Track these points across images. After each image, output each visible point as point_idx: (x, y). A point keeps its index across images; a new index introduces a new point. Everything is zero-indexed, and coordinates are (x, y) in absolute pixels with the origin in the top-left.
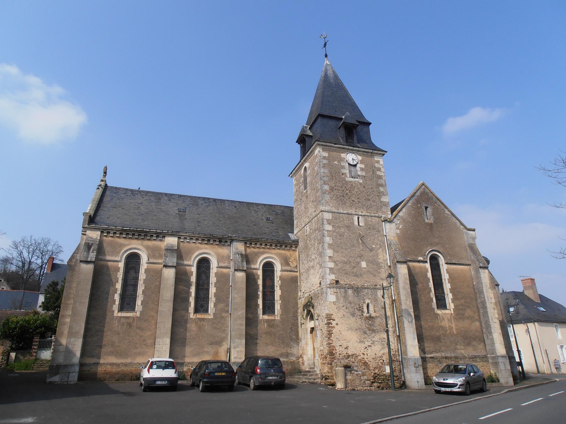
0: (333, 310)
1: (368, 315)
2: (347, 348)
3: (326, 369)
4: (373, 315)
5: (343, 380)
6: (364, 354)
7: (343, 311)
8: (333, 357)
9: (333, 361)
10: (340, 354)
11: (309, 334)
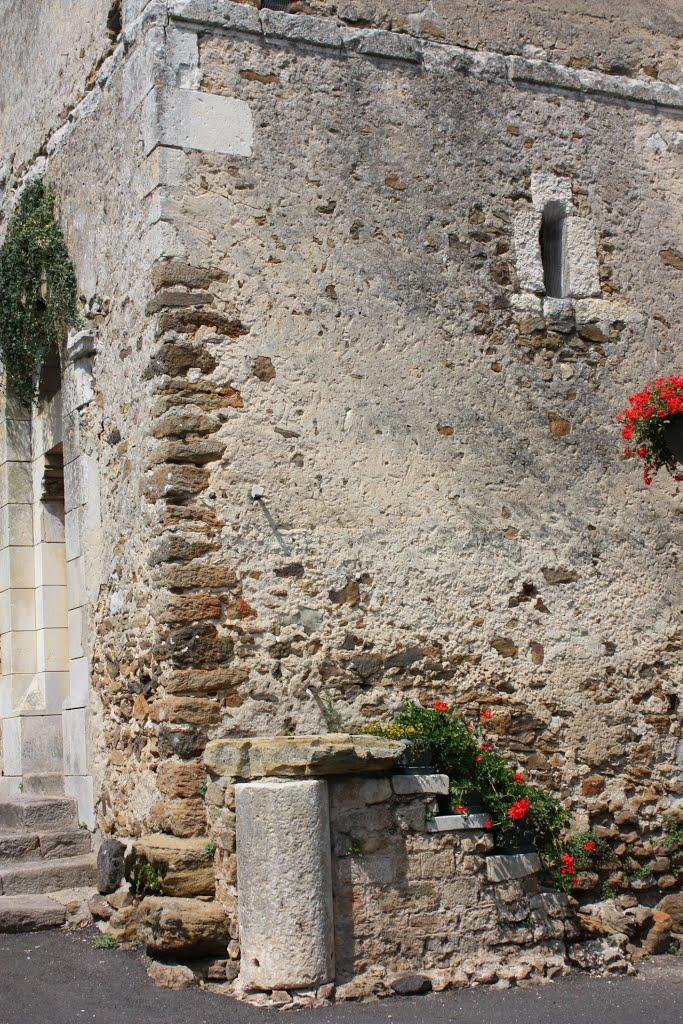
0: (224, 236)
1: (549, 306)
2: (351, 592)
3: (146, 794)
4: (599, 311)
5: (306, 902)
6: (505, 647)
7: (323, 257)
8: (215, 676)
9: (215, 719)
10: (281, 650)
11: (39, 509)
